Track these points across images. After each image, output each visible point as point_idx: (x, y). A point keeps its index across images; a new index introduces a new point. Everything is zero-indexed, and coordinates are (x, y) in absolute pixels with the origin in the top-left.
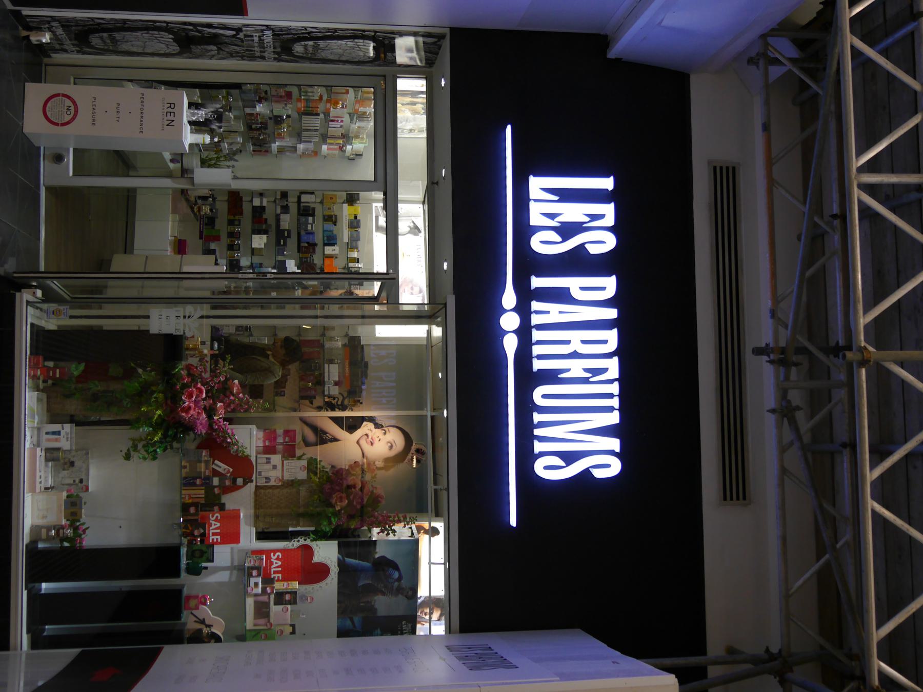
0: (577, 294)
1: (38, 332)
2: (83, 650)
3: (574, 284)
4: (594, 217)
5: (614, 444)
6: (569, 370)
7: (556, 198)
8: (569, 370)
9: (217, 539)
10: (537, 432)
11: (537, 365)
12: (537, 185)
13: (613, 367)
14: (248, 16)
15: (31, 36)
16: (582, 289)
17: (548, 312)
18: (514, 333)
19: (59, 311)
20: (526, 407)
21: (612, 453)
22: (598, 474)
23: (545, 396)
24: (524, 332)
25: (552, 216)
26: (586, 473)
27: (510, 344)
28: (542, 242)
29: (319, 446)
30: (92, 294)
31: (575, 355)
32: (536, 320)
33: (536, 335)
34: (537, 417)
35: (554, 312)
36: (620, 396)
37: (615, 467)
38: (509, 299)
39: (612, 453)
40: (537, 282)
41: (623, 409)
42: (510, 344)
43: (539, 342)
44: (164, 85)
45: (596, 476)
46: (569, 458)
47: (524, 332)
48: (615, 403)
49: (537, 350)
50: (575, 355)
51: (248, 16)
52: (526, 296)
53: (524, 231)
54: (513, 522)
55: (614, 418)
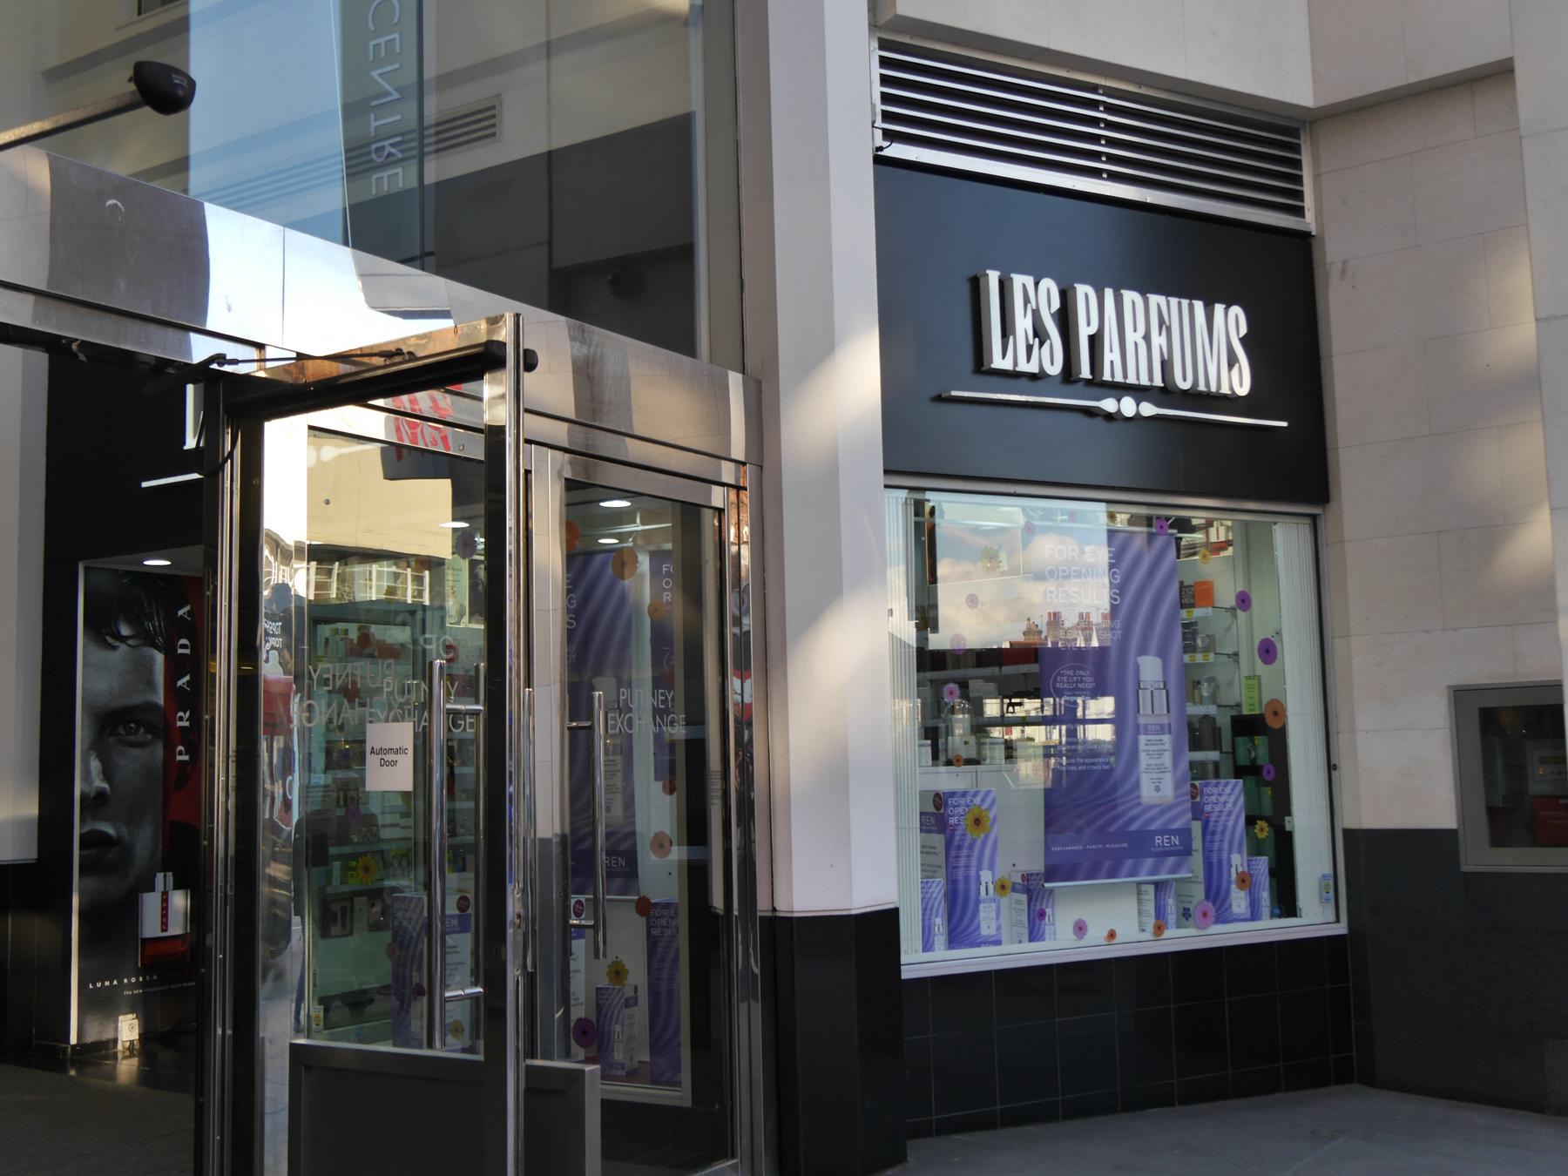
0: (1093, 330)
1: (611, 1109)
2: (574, 1039)
3: (1084, 332)
4: (1027, 301)
5: (1219, 309)
6: (1160, 346)
7: (1011, 338)
8: (1160, 346)
11: (1158, 382)
13: (1155, 299)
16: (1089, 325)
17: (1112, 362)
22: (1244, 330)
23: (1185, 379)
25: (1029, 348)
26: (1243, 340)
28: (1052, 364)
30: (503, 1012)
31: (1147, 338)
35: (1111, 355)
36: (1180, 297)
40: (1086, 373)
41: (1191, 297)
43: (1113, 375)
44: (235, 894)
50: (1147, 338)
52: (1099, 385)
54: (145, 484)
55: (1199, 306)
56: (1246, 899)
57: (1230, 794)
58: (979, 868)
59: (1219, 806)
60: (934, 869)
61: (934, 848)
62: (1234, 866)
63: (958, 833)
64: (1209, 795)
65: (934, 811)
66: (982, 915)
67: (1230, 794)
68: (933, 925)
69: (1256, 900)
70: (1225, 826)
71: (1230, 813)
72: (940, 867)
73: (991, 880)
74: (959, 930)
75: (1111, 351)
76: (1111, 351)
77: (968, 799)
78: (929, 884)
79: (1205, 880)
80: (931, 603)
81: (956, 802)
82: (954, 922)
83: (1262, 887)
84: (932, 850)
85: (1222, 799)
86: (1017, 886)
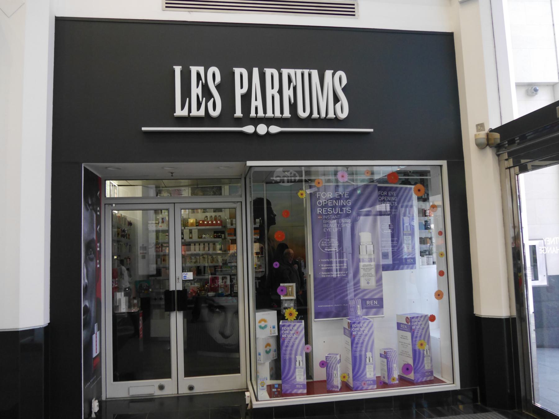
3: (239, 92)
5: (328, 74)
9: (372, 302)
10: (323, 115)
12: (179, 112)
14: (115, 379)
15: (95, 412)
16: (242, 87)
18: (267, 132)
19: (262, 383)
20: (309, 121)
21: (333, 74)
24: (269, 121)
27: (274, 129)
29: (331, 237)
31: (280, 92)
32: (261, 114)
33: (269, 114)
34: (315, 115)
35: (256, 103)
36: (303, 69)
37: (341, 73)
38: (249, 129)
39: (333, 74)
40: (238, 113)
42: (274, 129)
45: (346, 83)
46: (336, 99)
47: (269, 121)
48: (306, 72)
49: (278, 114)
50: (280, 92)
51: (115, 379)
52: (247, 119)
53: (207, 119)
56: (304, 375)
57: (423, 321)
58: (366, 351)
59: (418, 326)
60: (407, 345)
61: (407, 337)
62: (425, 350)
63: (416, 332)
64: (285, 330)
65: (405, 323)
66: (367, 369)
67: (423, 321)
68: (333, 374)
69: (330, 375)
70: (364, 340)
71: (366, 335)
72: (409, 344)
73: (428, 348)
74: (358, 375)
75: (256, 100)
76: (256, 100)
77: (419, 319)
78: (331, 358)
79: (413, 356)
80: (160, 241)
81: (285, 328)
82: (355, 373)
83: (393, 363)
84: (405, 338)
85: (419, 323)
86: (382, 355)
